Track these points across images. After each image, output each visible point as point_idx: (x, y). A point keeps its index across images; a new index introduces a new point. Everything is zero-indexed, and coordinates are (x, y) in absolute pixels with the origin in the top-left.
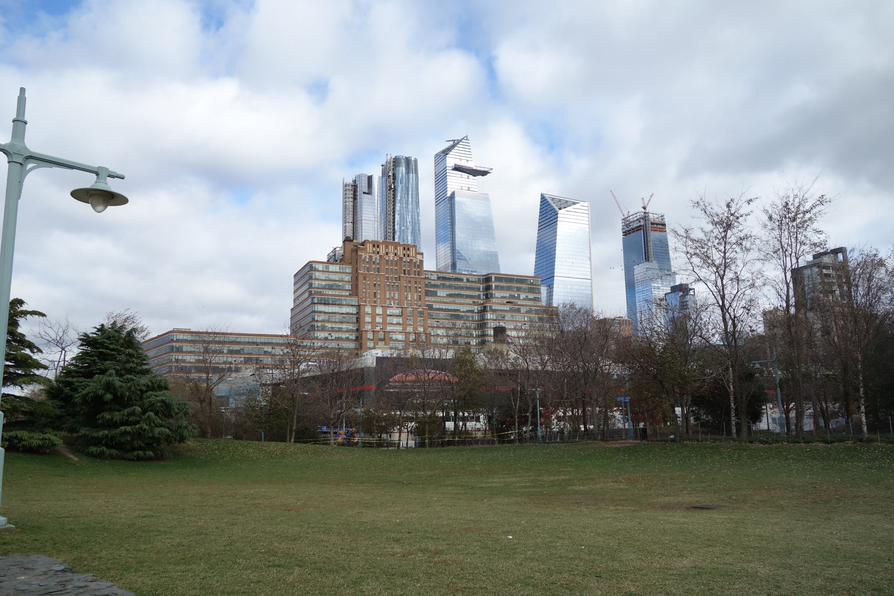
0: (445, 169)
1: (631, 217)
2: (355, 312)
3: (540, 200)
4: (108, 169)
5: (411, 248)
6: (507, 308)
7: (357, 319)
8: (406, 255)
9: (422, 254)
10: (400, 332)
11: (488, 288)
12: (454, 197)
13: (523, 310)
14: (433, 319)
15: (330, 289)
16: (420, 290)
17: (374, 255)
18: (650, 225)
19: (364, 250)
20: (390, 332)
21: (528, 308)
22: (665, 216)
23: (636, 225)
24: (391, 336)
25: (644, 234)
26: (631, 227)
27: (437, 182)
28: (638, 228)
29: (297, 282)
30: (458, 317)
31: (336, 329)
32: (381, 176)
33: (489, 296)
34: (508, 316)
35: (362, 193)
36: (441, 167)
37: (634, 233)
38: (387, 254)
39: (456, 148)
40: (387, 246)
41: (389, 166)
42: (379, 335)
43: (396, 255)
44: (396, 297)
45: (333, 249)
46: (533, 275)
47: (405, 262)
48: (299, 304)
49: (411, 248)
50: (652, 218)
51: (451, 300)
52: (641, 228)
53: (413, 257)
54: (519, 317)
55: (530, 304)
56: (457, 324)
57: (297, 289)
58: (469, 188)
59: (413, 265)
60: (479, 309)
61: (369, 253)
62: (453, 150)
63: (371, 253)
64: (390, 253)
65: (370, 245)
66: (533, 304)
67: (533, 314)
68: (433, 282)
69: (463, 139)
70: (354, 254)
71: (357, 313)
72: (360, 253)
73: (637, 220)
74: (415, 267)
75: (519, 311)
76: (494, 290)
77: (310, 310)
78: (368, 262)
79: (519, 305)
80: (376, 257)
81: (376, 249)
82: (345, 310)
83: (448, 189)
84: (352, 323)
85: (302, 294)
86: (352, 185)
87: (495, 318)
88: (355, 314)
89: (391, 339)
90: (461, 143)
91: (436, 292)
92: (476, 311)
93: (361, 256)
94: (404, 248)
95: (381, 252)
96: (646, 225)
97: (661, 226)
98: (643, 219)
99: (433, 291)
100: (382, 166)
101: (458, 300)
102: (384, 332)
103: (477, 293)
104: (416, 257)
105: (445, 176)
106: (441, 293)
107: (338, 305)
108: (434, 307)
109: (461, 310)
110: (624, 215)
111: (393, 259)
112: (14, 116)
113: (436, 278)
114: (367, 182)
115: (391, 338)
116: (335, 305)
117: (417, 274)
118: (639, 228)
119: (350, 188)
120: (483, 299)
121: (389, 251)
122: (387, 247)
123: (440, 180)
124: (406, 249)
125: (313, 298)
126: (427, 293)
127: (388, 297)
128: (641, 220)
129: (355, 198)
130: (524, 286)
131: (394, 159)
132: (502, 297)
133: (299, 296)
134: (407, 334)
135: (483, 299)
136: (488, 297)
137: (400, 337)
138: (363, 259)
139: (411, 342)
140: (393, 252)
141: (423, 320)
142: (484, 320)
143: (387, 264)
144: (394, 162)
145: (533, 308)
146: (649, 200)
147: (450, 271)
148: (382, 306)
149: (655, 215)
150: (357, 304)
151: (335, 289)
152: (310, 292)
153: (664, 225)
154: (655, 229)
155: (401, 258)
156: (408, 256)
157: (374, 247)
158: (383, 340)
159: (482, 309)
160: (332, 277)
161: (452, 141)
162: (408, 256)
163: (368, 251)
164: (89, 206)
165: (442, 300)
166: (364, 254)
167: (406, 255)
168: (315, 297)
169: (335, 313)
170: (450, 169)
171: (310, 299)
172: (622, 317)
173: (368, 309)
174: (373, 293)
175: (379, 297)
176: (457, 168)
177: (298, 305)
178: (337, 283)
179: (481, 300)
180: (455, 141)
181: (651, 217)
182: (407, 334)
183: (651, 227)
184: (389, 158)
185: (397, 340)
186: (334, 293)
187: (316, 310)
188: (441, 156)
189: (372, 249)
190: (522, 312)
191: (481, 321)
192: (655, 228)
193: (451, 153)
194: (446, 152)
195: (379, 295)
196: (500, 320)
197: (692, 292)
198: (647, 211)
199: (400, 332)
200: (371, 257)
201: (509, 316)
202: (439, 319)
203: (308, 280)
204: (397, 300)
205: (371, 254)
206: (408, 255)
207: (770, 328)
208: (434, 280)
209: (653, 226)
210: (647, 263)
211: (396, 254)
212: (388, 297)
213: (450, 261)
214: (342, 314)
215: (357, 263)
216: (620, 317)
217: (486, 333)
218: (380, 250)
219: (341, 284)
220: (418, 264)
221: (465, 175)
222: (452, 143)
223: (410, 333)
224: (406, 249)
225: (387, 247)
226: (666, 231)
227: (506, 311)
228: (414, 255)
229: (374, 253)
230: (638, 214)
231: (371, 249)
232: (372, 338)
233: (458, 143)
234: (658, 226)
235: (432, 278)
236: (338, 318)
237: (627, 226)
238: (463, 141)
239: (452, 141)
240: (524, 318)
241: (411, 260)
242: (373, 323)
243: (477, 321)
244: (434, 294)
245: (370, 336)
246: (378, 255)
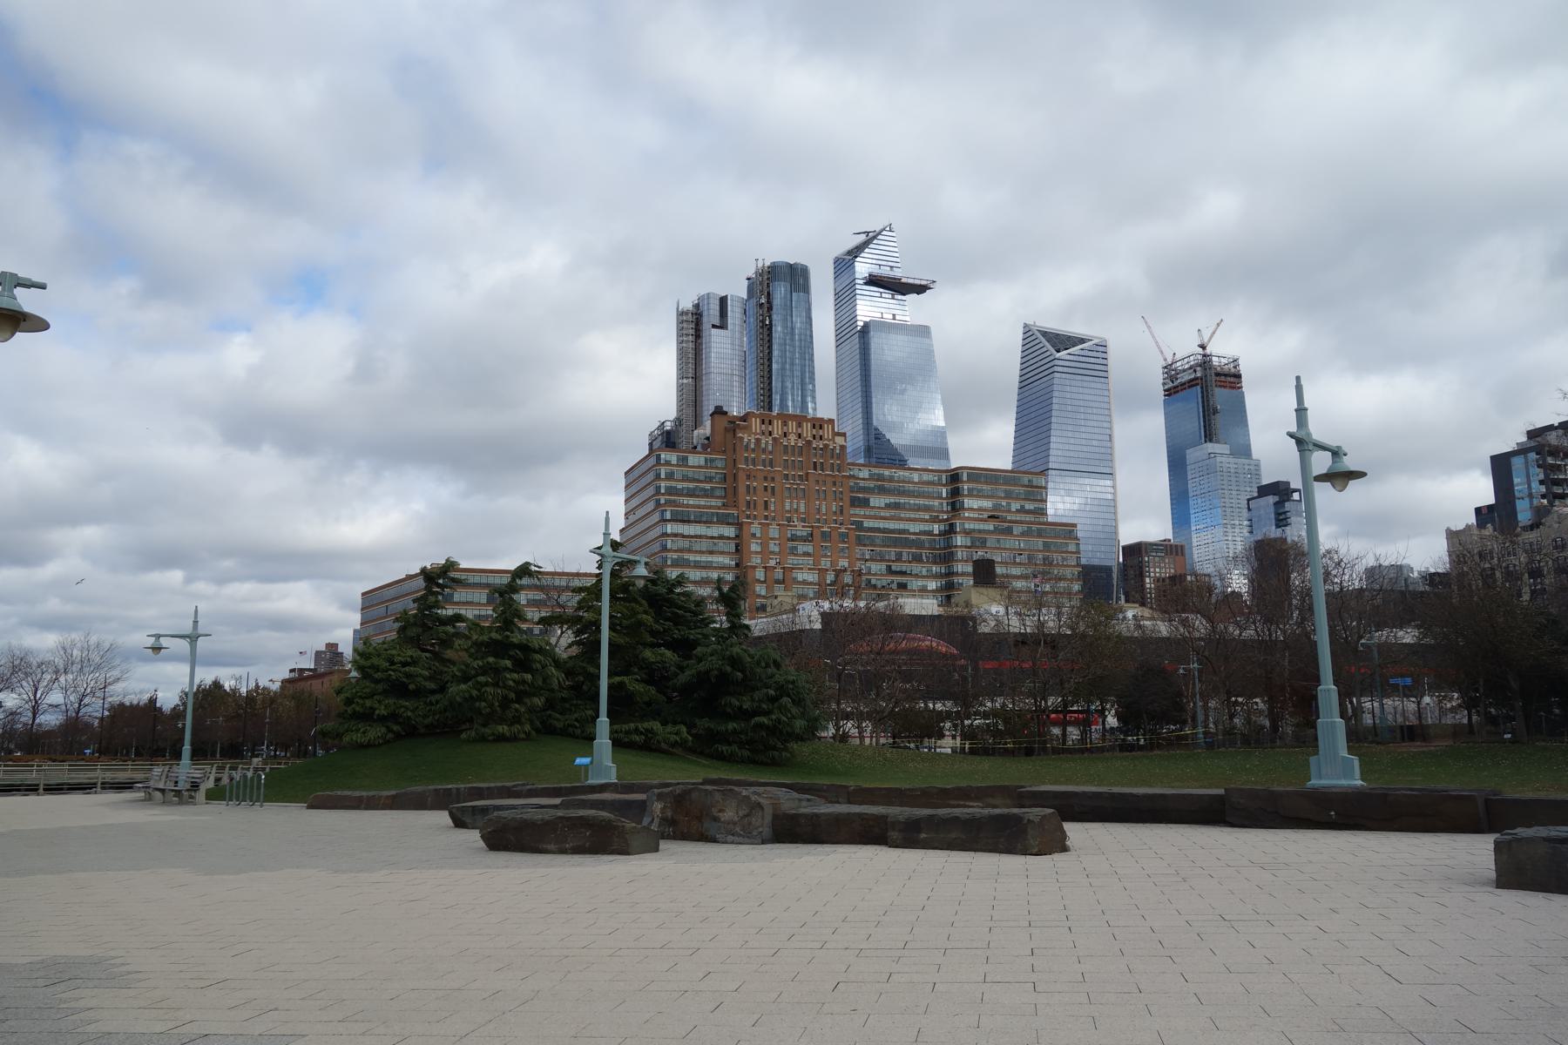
0: (852, 283)
2: (733, 535)
3: (1021, 336)
4: (16, 275)
5: (826, 426)
6: (990, 526)
7: (737, 547)
10: (809, 569)
11: (955, 493)
12: (868, 332)
13: (1017, 529)
15: (691, 496)
17: (763, 437)
18: (1214, 378)
19: (747, 429)
23: (1186, 377)
24: (794, 575)
25: (1202, 392)
26: (1179, 381)
27: (839, 305)
28: (1191, 383)
31: (702, 564)
32: (745, 297)
34: (991, 541)
36: (845, 280)
38: (785, 436)
42: (776, 574)
43: (800, 437)
44: (802, 509)
47: (815, 449)
48: (635, 522)
50: (1217, 364)
51: (893, 512)
52: (1197, 381)
53: (829, 440)
54: (1010, 542)
55: (1028, 519)
57: (631, 497)
58: (894, 315)
59: (829, 454)
60: (942, 528)
61: (756, 434)
62: (867, 250)
63: (758, 434)
65: (778, 422)
68: (862, 483)
69: (884, 229)
70: (729, 436)
71: (737, 536)
72: (740, 435)
73: (1190, 368)
74: (832, 457)
76: (966, 496)
77: (657, 531)
78: (753, 450)
79: (1010, 522)
80: (766, 442)
83: (858, 318)
84: (729, 553)
85: (642, 504)
87: (969, 544)
89: (795, 581)
90: (880, 237)
91: (869, 499)
92: (936, 532)
94: (814, 425)
96: (1206, 376)
97: (1232, 379)
98: (1200, 366)
100: (748, 279)
102: (784, 568)
104: (833, 440)
105: (853, 299)
106: (877, 501)
107: (705, 522)
108: (865, 525)
109: (912, 530)
110: (1165, 360)
114: (718, 308)
115: (795, 579)
118: (1194, 382)
119: (690, 317)
120: (947, 512)
121: (788, 429)
122: (785, 424)
123: (843, 302)
124: (817, 426)
126: (855, 502)
127: (788, 508)
128: (1198, 368)
129: (698, 334)
130: (1017, 489)
131: (769, 267)
132: (980, 509)
133: (637, 507)
134: (822, 572)
135: (947, 512)
136: (956, 507)
137: (812, 577)
138: (745, 444)
139: (829, 585)
141: (847, 547)
143: (786, 452)
145: (1034, 527)
146: (1214, 333)
147: (861, 461)
149: (1223, 360)
151: (698, 496)
152: (658, 502)
153: (1239, 376)
155: (809, 443)
156: (821, 439)
157: (814, 428)
158: (783, 582)
160: (690, 473)
161: (864, 233)
162: (821, 439)
163: (754, 431)
165: (877, 514)
169: (700, 537)
170: (862, 282)
171: (657, 514)
172: (1170, 540)
173: (755, 528)
176: (873, 281)
177: (632, 524)
178: (702, 485)
179: (945, 512)
180: (868, 233)
182: (822, 572)
184: (760, 265)
185: (805, 582)
186: (697, 503)
187: (669, 531)
189: (761, 427)
190: (1015, 533)
191: (945, 549)
193: (862, 255)
194: (856, 252)
196: (978, 547)
198: (1208, 351)
200: (758, 441)
202: (875, 546)
204: (803, 513)
205: (758, 436)
206: (821, 436)
207: (1107, 618)
208: (863, 479)
209: (1218, 378)
211: (800, 436)
212: (788, 508)
213: (861, 443)
214: (712, 538)
215: (734, 450)
216: (1165, 541)
218: (773, 428)
220: (838, 451)
221: (887, 294)
222: (863, 238)
223: (827, 570)
224: (817, 426)
225: (785, 424)
227: (989, 532)
228: (830, 437)
229: (763, 434)
230: (1192, 358)
232: (762, 579)
233: (875, 237)
234: (1229, 379)
235: (861, 475)
237: (1172, 378)
238: (884, 233)
239: (864, 233)
240: (1019, 544)
241: (826, 446)
242: (765, 553)
244: (865, 503)
245: (760, 574)
246: (770, 438)
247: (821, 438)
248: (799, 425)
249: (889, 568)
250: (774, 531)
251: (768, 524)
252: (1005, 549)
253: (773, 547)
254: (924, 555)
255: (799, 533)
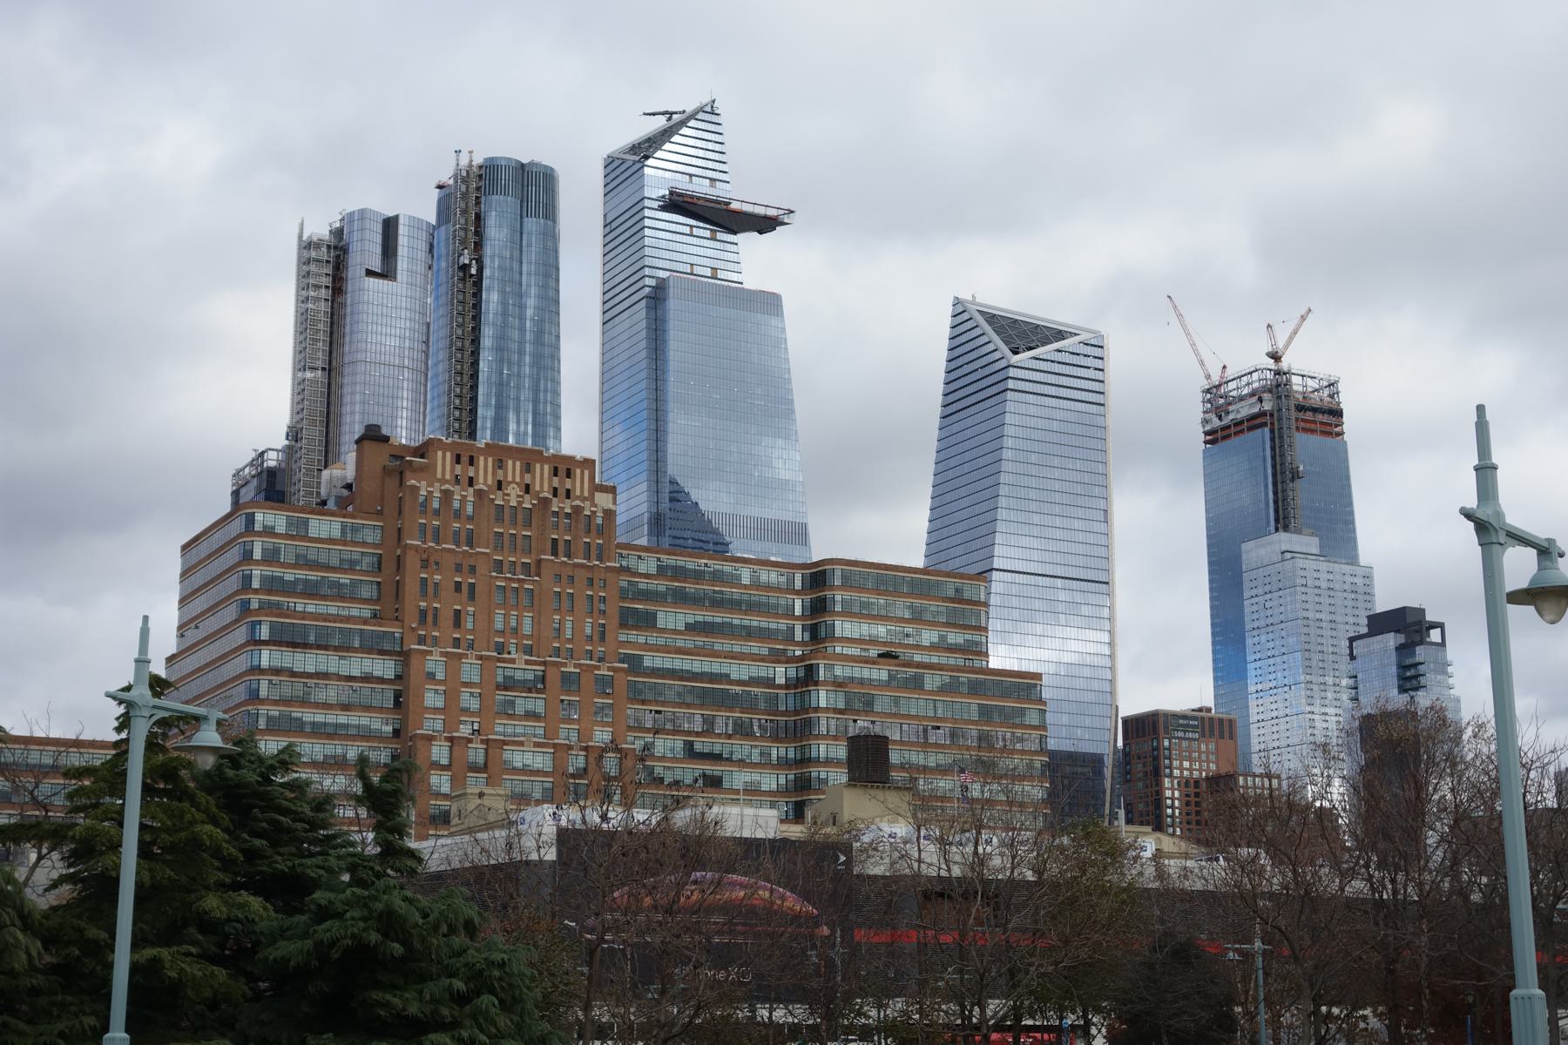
0: (640, 202)
1: (1232, 385)
5: (578, 471)
8: (562, 492)
9: (612, 490)
10: (537, 745)
11: (819, 607)
13: (932, 681)
14: (643, 702)
15: (311, 596)
16: (602, 607)
18: (1294, 414)
19: (427, 471)
20: (505, 743)
21: (946, 677)
22: (1341, 386)
23: (1245, 410)
25: (1273, 439)
26: (1231, 417)
28: (1254, 422)
29: (194, 567)
30: (725, 700)
33: (823, 634)
35: (364, 273)
36: (625, 198)
37: (1242, 437)
38: (500, 488)
39: (676, 138)
40: (501, 461)
41: (464, 188)
44: (527, 629)
45: (253, 455)
46: (918, 561)
47: (556, 514)
49: (578, 471)
50: (1300, 389)
51: (700, 640)
53: (584, 499)
55: (952, 662)
56: (719, 720)
59: (582, 526)
60: (792, 673)
61: (443, 481)
62: (667, 146)
63: (447, 482)
64: (511, 482)
66: (961, 662)
67: (961, 694)
68: (643, 584)
69: (701, 110)
70: (392, 483)
71: (398, 677)
73: (1252, 394)
74: (588, 531)
75: (916, 684)
77: (241, 663)
78: (437, 513)
79: (919, 665)
80: (463, 497)
81: (465, 471)
82: (356, 665)
84: (381, 709)
85: (212, 609)
86: (329, 247)
87: (841, 705)
88: (389, 681)
91: (654, 615)
92: (780, 680)
93: (415, 489)
95: (481, 480)
96: (1280, 410)
97: (1325, 418)
98: (1270, 391)
99: (647, 612)
100: (440, 187)
101: (721, 644)
102: (487, 742)
103: (783, 624)
104: (591, 498)
106: (671, 618)
107: (336, 649)
108: (647, 663)
109: (734, 676)
110: (1208, 377)
111: (520, 503)
112: (1476, 462)
113: (653, 571)
116: (326, 648)
117: (429, 535)
119: (323, 253)
120: (803, 643)
122: (500, 464)
124: (562, 472)
125: (254, 624)
126: (631, 619)
127: (499, 625)
128: (1266, 396)
136: (818, 635)
138: (421, 499)
140: (518, 480)
142: (806, 709)
143: (500, 519)
144: (480, 176)
147: (643, 541)
148: (480, 658)
149: (1310, 382)
150: (399, 650)
151: (324, 597)
153: (1338, 413)
154: (1308, 426)
155: (545, 502)
156: (568, 496)
157: (458, 462)
158: (485, 768)
159: (801, 674)
161: (663, 113)
162: (568, 496)
163: (439, 476)
164: (1532, 608)
166: (424, 483)
167: (562, 492)
168: (260, 622)
170: (656, 204)
172: (1209, 710)
173: (435, 663)
174: (452, 614)
175: (470, 626)
176: (677, 203)
178: (333, 576)
179: (798, 644)
180: (672, 113)
181: (1295, 388)
182: (560, 751)
183: (1297, 419)
184: (464, 161)
185: (526, 770)
186: (322, 610)
188: (624, 161)
189: (453, 470)
190: (927, 687)
191: (796, 712)
192: (1308, 421)
193: (659, 154)
194: (646, 148)
195: (470, 619)
196: (858, 712)
197: (1435, 635)
198: (1285, 364)
199: (537, 745)
200: (447, 496)
201: (887, 700)
202: (663, 703)
203: (239, 564)
205: (447, 486)
206: (568, 491)
208: (647, 576)
209: (1301, 415)
210: (1283, 535)
211: (527, 489)
212: (499, 625)
213: (644, 508)
214: (350, 678)
215: (400, 512)
217: (814, 754)
218: (477, 472)
219: (345, 579)
220: (599, 521)
221: (703, 230)
222: (660, 122)
223: (570, 747)
224: (562, 472)
226: (1341, 434)
228: (586, 494)
230: (1255, 376)
231: (448, 468)
232: (445, 761)
233: (683, 123)
234: (1320, 417)
235: (642, 569)
236: (331, 693)
239: (663, 113)
243: (786, 713)
246: (471, 490)
247: (568, 494)
248: (528, 468)
249: (689, 746)
250: (470, 670)
251: (460, 656)
252: (909, 716)
253: (469, 700)
254: (756, 724)
255: (519, 675)
